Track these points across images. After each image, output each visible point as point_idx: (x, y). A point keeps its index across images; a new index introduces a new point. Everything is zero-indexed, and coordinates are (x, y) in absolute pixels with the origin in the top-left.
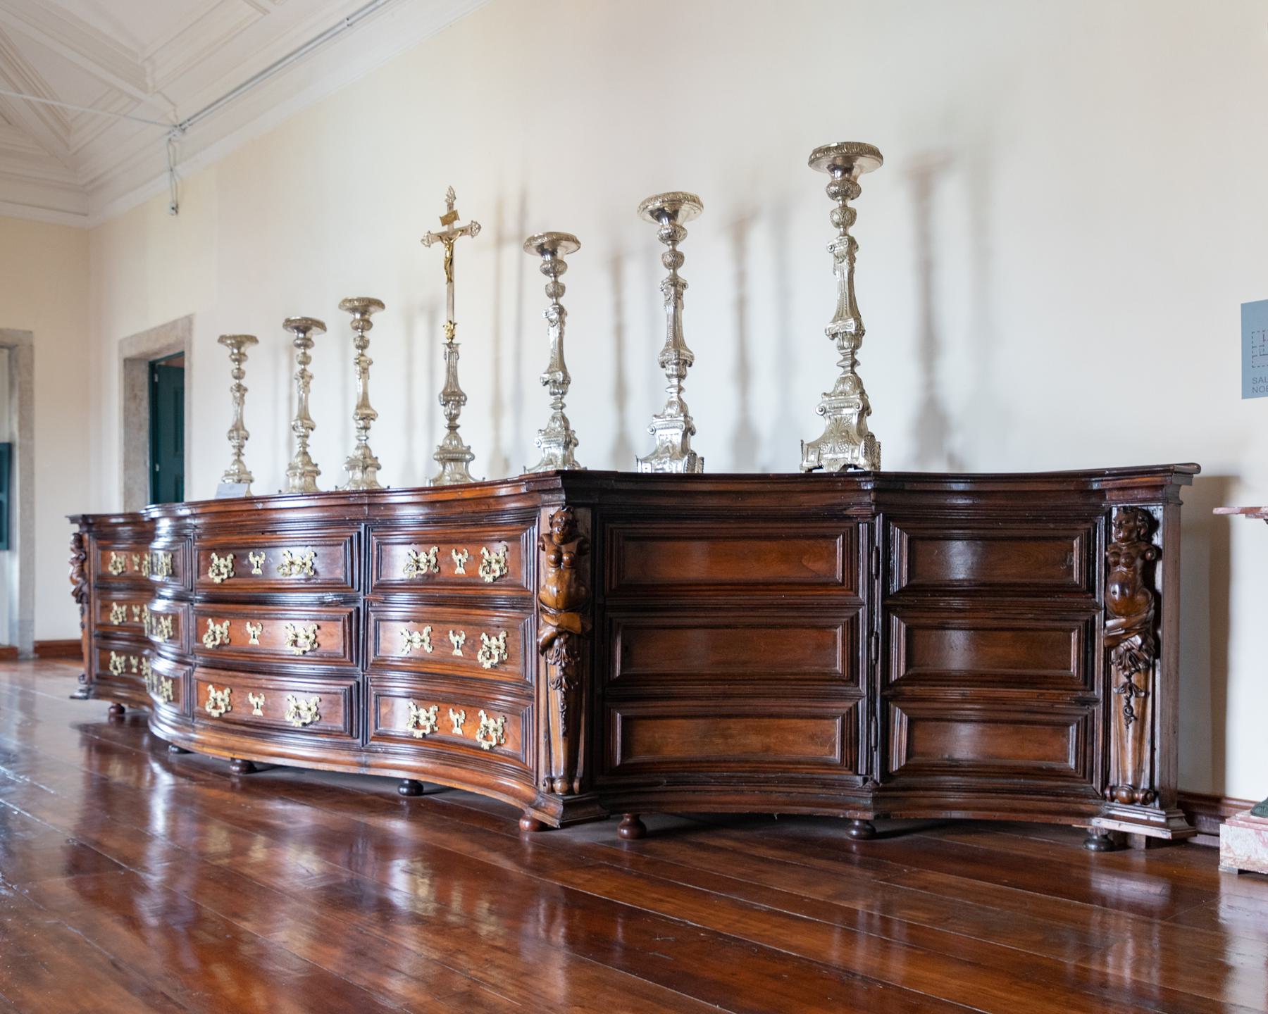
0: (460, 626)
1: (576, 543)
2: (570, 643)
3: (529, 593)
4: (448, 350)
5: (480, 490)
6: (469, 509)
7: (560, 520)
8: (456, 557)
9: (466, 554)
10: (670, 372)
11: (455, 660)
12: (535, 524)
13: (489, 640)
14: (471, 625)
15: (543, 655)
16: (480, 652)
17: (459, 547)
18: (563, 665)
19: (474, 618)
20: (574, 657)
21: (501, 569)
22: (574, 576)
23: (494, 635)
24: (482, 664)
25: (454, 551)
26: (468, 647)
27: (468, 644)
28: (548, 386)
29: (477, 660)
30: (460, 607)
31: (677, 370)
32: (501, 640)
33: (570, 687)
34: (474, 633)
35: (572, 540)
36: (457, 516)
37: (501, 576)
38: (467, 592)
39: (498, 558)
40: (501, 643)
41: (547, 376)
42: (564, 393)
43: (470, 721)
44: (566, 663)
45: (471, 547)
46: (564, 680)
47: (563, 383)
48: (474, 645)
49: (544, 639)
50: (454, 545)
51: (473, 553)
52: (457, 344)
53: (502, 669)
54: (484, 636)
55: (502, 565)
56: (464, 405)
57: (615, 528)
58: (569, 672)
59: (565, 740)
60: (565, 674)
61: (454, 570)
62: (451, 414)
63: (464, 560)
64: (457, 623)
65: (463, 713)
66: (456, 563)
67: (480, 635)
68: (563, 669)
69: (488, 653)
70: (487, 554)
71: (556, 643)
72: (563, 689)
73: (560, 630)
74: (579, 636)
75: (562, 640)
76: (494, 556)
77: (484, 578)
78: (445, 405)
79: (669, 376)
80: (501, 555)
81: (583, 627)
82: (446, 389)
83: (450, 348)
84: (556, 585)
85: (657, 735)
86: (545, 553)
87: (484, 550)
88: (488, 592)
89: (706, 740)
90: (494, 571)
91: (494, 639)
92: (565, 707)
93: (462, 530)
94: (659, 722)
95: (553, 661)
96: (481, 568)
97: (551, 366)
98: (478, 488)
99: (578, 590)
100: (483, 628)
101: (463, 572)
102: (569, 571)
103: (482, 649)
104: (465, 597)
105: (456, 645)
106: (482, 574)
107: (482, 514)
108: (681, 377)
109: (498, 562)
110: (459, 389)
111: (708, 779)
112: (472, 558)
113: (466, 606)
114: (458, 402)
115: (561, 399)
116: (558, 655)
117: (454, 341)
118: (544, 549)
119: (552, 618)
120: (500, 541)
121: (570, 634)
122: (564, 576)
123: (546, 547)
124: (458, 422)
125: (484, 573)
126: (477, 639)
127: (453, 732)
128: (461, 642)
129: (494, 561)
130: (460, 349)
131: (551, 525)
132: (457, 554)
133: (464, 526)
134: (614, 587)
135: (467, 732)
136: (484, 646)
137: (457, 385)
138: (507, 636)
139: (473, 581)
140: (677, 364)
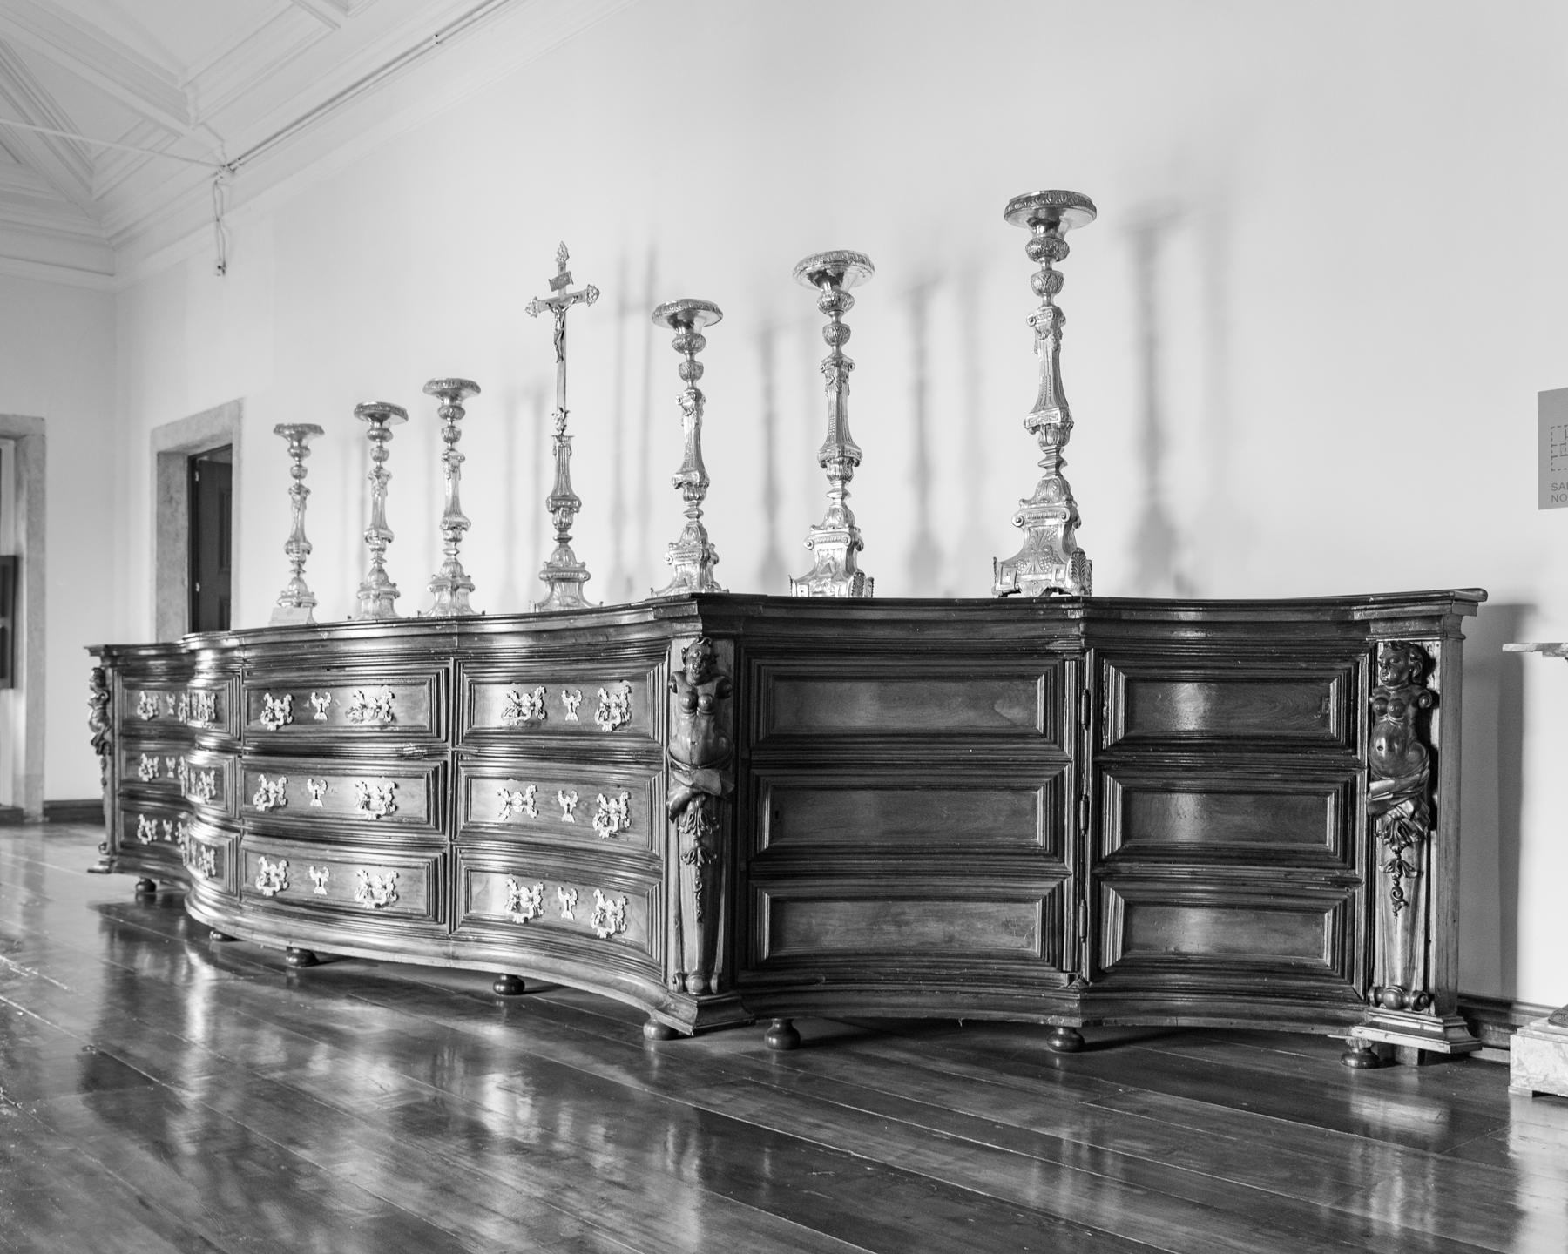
0: (571, 786)
2: (707, 806)
3: (657, 745)
5: (598, 617)
7: (695, 655)
8: (566, 701)
9: (579, 696)
10: (832, 473)
16: (596, 818)
17: (571, 687)
18: (699, 834)
19: (589, 775)
20: (712, 824)
21: (623, 716)
22: (712, 725)
23: (613, 796)
24: (599, 832)
25: (564, 692)
26: (582, 811)
27: (582, 807)
30: (571, 761)
31: (841, 470)
32: (622, 803)
37: (623, 724)
39: (618, 701)
41: (680, 478)
42: (700, 498)
43: (583, 902)
48: (588, 809)
49: (675, 802)
52: (570, 437)
53: (623, 838)
55: (624, 710)
59: (700, 926)
60: (701, 845)
62: (561, 523)
63: (576, 704)
65: (574, 892)
67: (596, 797)
68: (698, 839)
69: (606, 819)
70: (605, 696)
71: (690, 807)
72: (699, 864)
73: (694, 790)
74: (718, 798)
76: (613, 699)
78: (553, 512)
79: (831, 478)
80: (623, 697)
81: (723, 787)
82: (555, 491)
85: (814, 921)
90: (614, 718)
91: (613, 801)
93: (574, 667)
96: (597, 713)
97: (685, 465)
100: (600, 788)
102: (706, 718)
104: (578, 749)
106: (598, 721)
107: (599, 647)
108: (846, 479)
109: (619, 706)
112: (586, 701)
113: (579, 761)
116: (692, 822)
118: (675, 691)
120: (621, 681)
121: (707, 795)
124: (570, 533)
125: (602, 719)
126: (591, 802)
128: (573, 805)
130: (573, 443)
131: (685, 661)
132: (568, 697)
134: (761, 738)
137: (569, 488)
138: (629, 798)
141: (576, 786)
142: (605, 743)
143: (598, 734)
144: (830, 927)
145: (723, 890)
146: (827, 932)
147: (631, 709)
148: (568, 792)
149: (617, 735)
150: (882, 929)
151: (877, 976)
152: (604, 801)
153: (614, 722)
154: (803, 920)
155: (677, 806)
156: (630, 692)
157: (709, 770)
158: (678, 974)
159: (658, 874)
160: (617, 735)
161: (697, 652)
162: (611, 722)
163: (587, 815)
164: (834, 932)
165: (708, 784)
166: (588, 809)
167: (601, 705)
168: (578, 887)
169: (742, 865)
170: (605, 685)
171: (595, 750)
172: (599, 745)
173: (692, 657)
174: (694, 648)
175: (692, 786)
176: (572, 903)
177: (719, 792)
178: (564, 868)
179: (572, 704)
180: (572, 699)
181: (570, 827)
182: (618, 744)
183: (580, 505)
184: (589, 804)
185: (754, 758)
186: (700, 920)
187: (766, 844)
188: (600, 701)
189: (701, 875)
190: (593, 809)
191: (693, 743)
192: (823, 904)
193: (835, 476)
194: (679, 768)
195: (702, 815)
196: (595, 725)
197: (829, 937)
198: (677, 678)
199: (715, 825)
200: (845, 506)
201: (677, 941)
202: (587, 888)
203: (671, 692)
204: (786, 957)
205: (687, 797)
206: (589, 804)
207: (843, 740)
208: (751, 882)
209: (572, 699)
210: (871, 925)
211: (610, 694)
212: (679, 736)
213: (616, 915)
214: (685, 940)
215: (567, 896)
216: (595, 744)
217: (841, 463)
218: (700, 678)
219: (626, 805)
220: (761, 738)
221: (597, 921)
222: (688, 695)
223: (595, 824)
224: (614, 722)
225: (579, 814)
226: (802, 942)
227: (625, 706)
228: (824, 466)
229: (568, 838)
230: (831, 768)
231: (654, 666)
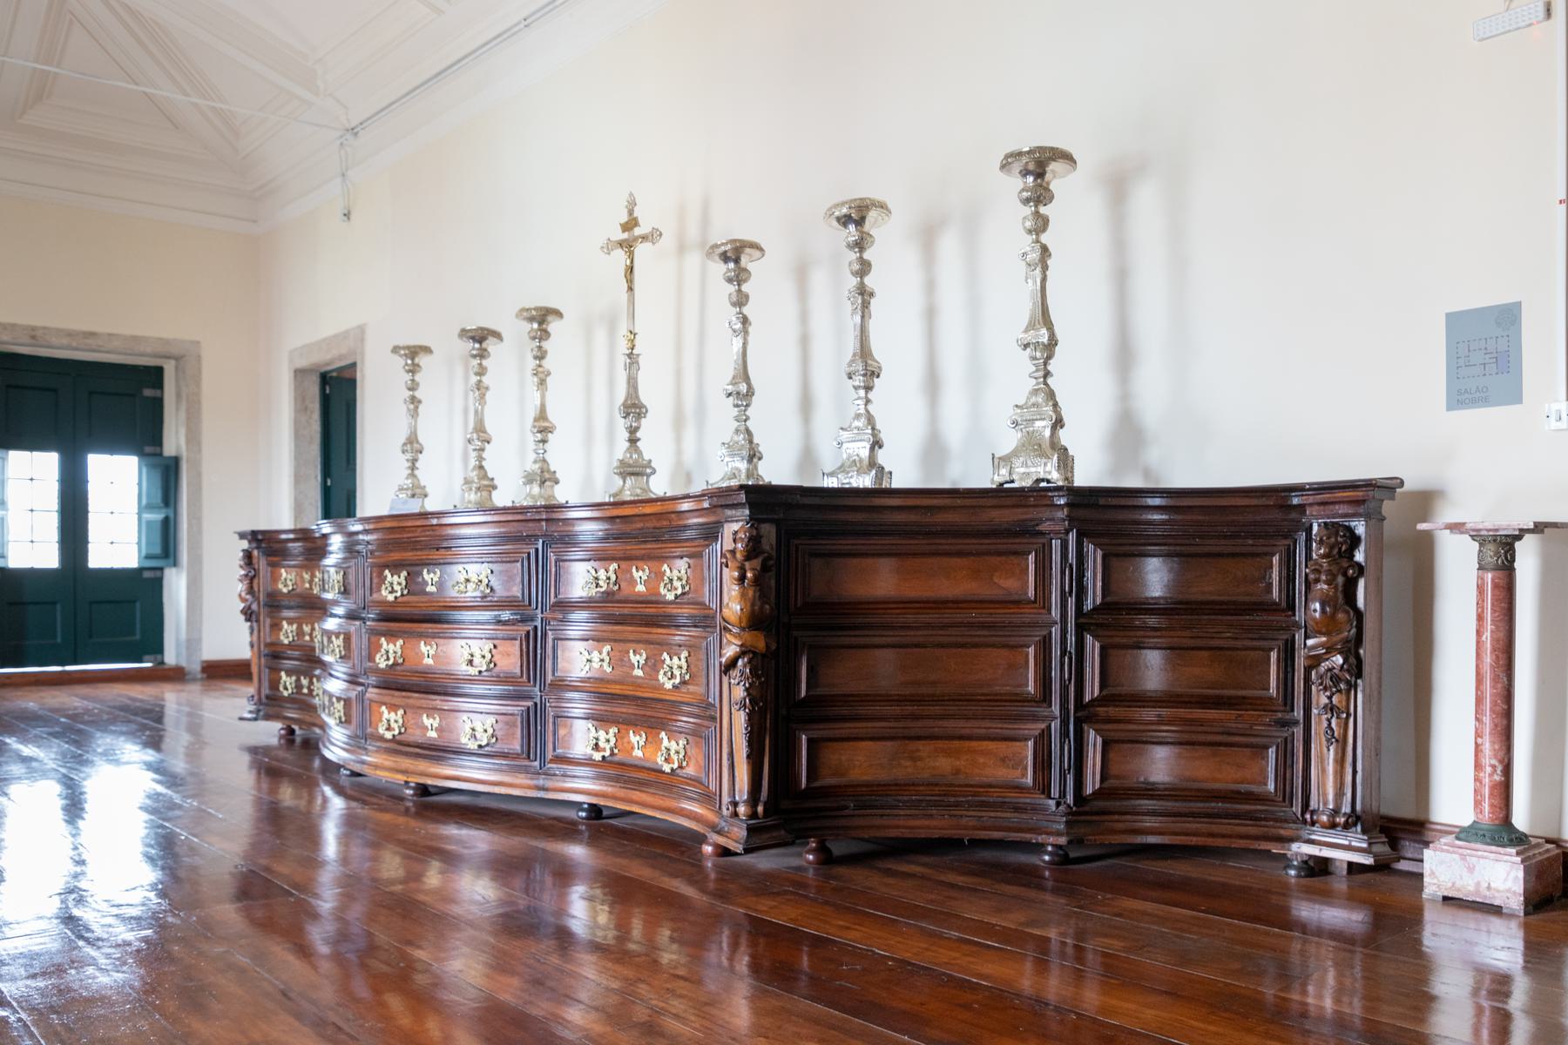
0: (641, 645)
2: (754, 663)
9: (647, 571)
10: (857, 383)
14: (653, 644)
16: (662, 672)
17: (640, 564)
19: (656, 636)
20: (758, 677)
21: (683, 587)
22: (758, 594)
23: (676, 654)
27: (649, 664)
28: (731, 398)
30: (641, 625)
31: (864, 381)
32: (683, 660)
33: (754, 708)
37: (683, 594)
38: (647, 610)
41: (730, 388)
48: (655, 665)
50: (635, 562)
52: (638, 355)
54: (665, 656)
55: (684, 582)
60: (749, 695)
63: (644, 578)
65: (644, 735)
68: (747, 690)
69: (670, 673)
71: (740, 663)
74: (764, 656)
76: (675, 573)
78: (625, 418)
79: (856, 388)
80: (683, 572)
82: (626, 400)
84: (740, 603)
87: (665, 567)
90: (676, 589)
91: (675, 659)
93: (643, 546)
94: (846, 744)
96: (662, 585)
99: (761, 608)
100: (664, 647)
102: (753, 588)
105: (636, 664)
106: (663, 591)
108: (868, 388)
109: (680, 579)
112: (653, 575)
113: (647, 625)
118: (727, 566)
121: (754, 653)
128: (642, 662)
130: (641, 360)
131: (735, 541)
132: (637, 571)
133: (645, 542)
135: (647, 755)
137: (637, 397)
139: (654, 598)
149: (677, 603)
151: (896, 803)
152: (668, 658)
162: (673, 593)
166: (655, 665)
175: (741, 646)
180: (641, 573)
181: (640, 681)
192: (851, 743)
194: (730, 631)
203: (724, 568)
209: (641, 573)
228: (850, 378)
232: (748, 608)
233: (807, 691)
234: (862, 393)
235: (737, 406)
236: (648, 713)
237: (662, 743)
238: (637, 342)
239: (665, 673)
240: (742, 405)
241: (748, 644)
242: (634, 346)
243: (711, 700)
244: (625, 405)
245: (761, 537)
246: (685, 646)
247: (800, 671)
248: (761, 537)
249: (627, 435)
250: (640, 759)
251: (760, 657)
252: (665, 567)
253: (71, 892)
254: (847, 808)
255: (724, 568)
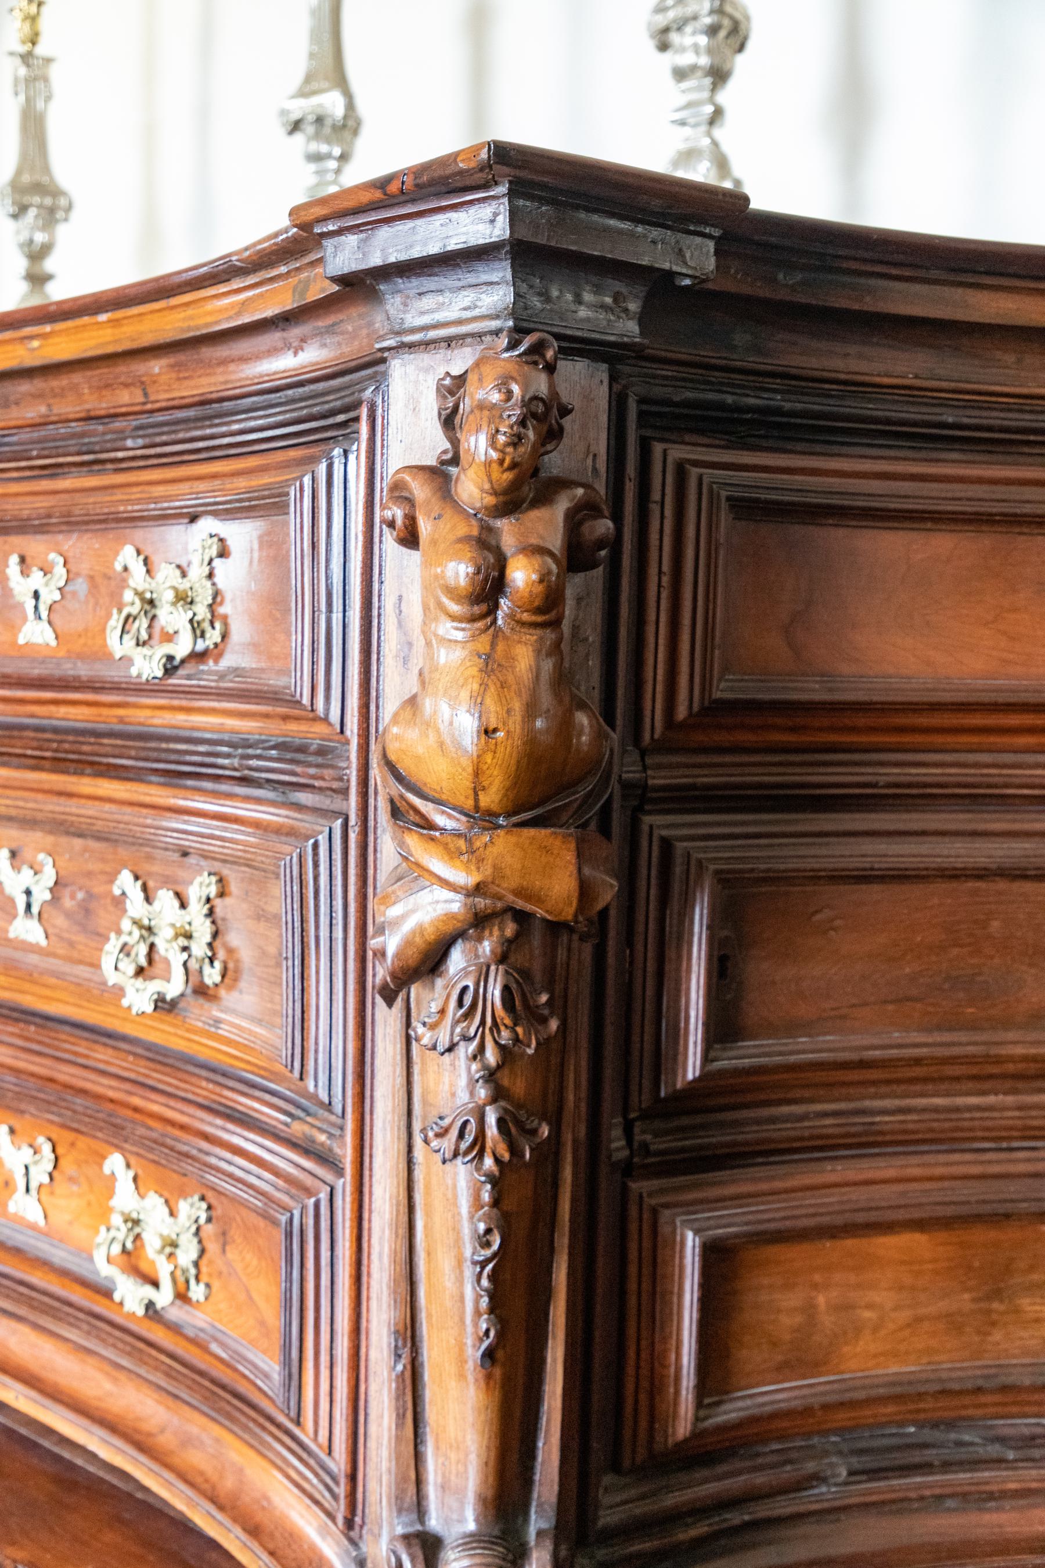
0: (37, 836)
1: (562, 505)
2: (518, 958)
3: (320, 729)
4: (23, 71)
5: (114, 323)
6: (67, 408)
7: (496, 397)
8: (21, 586)
9: (60, 571)
10: (687, 59)
11: (18, 955)
12: (352, 437)
13: (148, 899)
14: (80, 835)
15: (390, 1002)
16: (113, 945)
17: (34, 545)
18: (491, 1056)
19: (91, 809)
20: (536, 1018)
21: (197, 630)
22: (548, 665)
23: (167, 881)
24: (119, 991)
25: (14, 559)
26: (68, 915)
27: (68, 903)
28: (299, 138)
29: (97, 966)
30: (37, 764)
31: (710, 51)
32: (197, 910)
33: (514, 1150)
34: (91, 866)
35: (544, 497)
36: (25, 436)
37: (198, 656)
38: (62, 711)
39: (184, 585)
40: (196, 915)
41: (299, 107)
42: (344, 158)
43: (71, 1179)
44: (501, 1048)
45: (73, 543)
46: (491, 1118)
47: (344, 126)
48: (86, 910)
49: (408, 943)
50: (16, 540)
51: (85, 567)
52: (48, 61)
53: (197, 1012)
54: (125, 881)
55: (202, 611)
56: (66, 220)
57: (696, 463)
58: (518, 1085)
59: (489, 1377)
60: (498, 1095)
61: (14, 629)
62: (31, 241)
63: (50, 595)
64: (28, 823)
65: (46, 1148)
66: (20, 606)
67: (112, 878)
68: (491, 1076)
69: (143, 950)
70: (137, 568)
71: (457, 959)
72: (489, 1162)
73: (481, 903)
74: (555, 928)
75: (486, 947)
76: (167, 577)
77: (127, 660)
78: (15, 216)
79: (680, 74)
80: (197, 572)
81: (585, 891)
82: (19, 172)
83: (28, 65)
84: (478, 701)
85: (821, 1300)
86: (413, 558)
87: (127, 555)
88: (141, 715)
89: (995, 1305)
90: (169, 637)
91: (165, 898)
92: (496, 1241)
93: (46, 485)
94: (832, 1249)
95: (444, 1042)
96: (115, 622)
97: (308, 79)
98: (103, 317)
99: (565, 727)
100: (123, 852)
101: (49, 637)
102: (532, 637)
103: (119, 932)
104: (56, 730)
105: (21, 901)
106: (118, 646)
107: (118, 424)
108: (719, 75)
109: (184, 599)
110: (52, 179)
111: (994, 1450)
112: (81, 586)
113: (59, 764)
114: (52, 211)
115: (338, 171)
116: (468, 1015)
117: (40, 50)
118: (410, 539)
119: (452, 855)
120: (193, 519)
121: (522, 917)
122: (511, 658)
123: (425, 527)
124: (50, 265)
125: (129, 641)
126: (99, 889)
127: (12, 1208)
128: (41, 895)
129: (170, 595)
130: (55, 72)
131: (449, 421)
132: (25, 573)
133: (54, 471)
134: (682, 712)
135: (61, 1219)
136: (126, 925)
137: (46, 169)
138: (221, 894)
139: (84, 671)
140: (712, 31)
141: (50, 839)
142: (139, 716)
143: (116, 687)
144: (867, 1314)
145: (563, 1241)
146: (858, 1330)
147: (221, 610)
148: (27, 854)
149: (175, 692)
150: (1017, 1311)
151: (994, 1450)
152: (135, 892)
153: (168, 649)
154: (792, 1299)
155: (413, 957)
156: (223, 553)
157: (541, 834)
158: (406, 1538)
159: (326, 1159)
160: (175, 692)
161: (503, 385)
162: (162, 650)
163: (84, 928)
164: (875, 1329)
165: (538, 883)
166: (86, 910)
167: (128, 596)
168: (65, 1137)
169: (616, 1143)
170: (140, 534)
171: (111, 734)
172: (121, 720)
173: (481, 406)
174: (491, 373)
175: (478, 889)
176: (40, 1175)
177: (568, 913)
178: (16, 1071)
179: (36, 595)
180: (36, 579)
181: (33, 959)
182: (181, 718)
183: (69, 208)
184: (90, 896)
185: (656, 780)
186: (489, 1355)
187: (692, 1067)
188: (123, 584)
189: (496, 1203)
190: (103, 918)
191: (488, 732)
192: (850, 1243)
193: (694, 68)
194: (428, 825)
195: (506, 990)
196: (107, 656)
197: (867, 1344)
198: (420, 490)
199: (544, 1021)
200: (715, 143)
201: (400, 1417)
202: (82, 1142)
203: (389, 546)
204: (740, 1424)
205: (449, 928)
206: (90, 896)
207: (923, 720)
208: (634, 1186)
209: (36, 579)
210: (989, 1298)
211: (155, 559)
212: (427, 705)
213: (174, 1245)
214: (431, 1413)
215: (26, 1153)
216: (108, 718)
217: (712, 31)
218: (514, 486)
219: (211, 913)
220: (682, 712)
221: (116, 1249)
222: (468, 551)
223: (107, 963)
224: (168, 649)
225: (60, 921)
226: (785, 1369)
227: (204, 598)
228: (664, 46)
229: (27, 986)
230: (893, 809)
231: (314, 460)
232: (516, 722)
233: (706, 1059)
234: (697, 87)
235: (316, 158)
236: (66, 1073)
237: (110, 1192)
238: (45, 24)
239: (125, 949)
240: (329, 156)
241: (505, 888)
242: (36, 34)
243: (316, 1086)
244: (16, 186)
245: (565, 411)
246: (205, 856)
247: (679, 990)
248: (565, 411)
249: (21, 264)
250: (33, 1227)
251: (537, 940)
252: (127, 555)
253: (191, 603)
254: (818, 1478)
255: (389, 546)
